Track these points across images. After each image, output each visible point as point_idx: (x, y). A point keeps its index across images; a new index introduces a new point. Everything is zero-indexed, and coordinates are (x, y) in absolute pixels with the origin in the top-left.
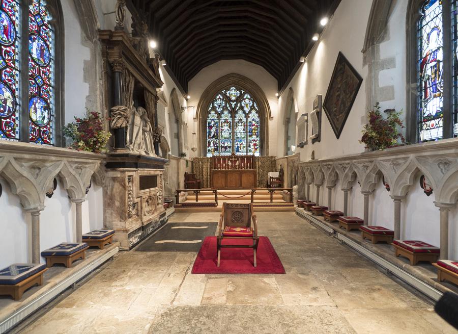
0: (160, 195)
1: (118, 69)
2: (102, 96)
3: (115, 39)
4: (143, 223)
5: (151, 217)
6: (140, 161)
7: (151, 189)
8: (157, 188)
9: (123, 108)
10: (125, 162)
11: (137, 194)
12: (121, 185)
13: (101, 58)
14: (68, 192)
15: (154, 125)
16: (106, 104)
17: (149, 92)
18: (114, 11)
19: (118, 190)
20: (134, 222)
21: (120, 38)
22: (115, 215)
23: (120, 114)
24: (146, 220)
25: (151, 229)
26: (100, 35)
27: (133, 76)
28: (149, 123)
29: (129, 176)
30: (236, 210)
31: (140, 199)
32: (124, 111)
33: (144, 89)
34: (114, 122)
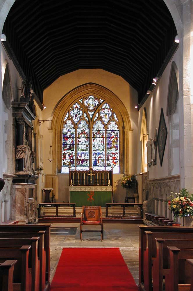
3: (21, 106)
9: (24, 147)
12: (22, 193)
19: (20, 197)
22: (17, 212)
34: (19, 155)
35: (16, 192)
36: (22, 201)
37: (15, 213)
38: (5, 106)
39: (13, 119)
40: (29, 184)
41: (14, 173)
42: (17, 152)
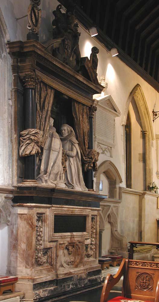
0: (91, 244)
1: (30, 84)
2: (11, 118)
3: (26, 50)
4: (57, 275)
5: (72, 271)
6: (55, 195)
7: (75, 233)
8: (85, 233)
9: (33, 132)
10: (33, 196)
11: (49, 236)
12: (28, 223)
13: (11, 73)
14: (111, 225)
15: (87, 147)
16: (15, 128)
17: (79, 103)
18: (26, 15)
19: (25, 230)
20: (44, 272)
21: (31, 49)
22: (21, 260)
23: (29, 139)
24: (62, 273)
25: (71, 286)
26: (10, 48)
27: (52, 88)
28: (77, 146)
29: (92, 215)
30: (144, 271)
31: (54, 244)
32: (34, 135)
33: (71, 101)
34: (23, 148)
35: (19, 220)
42: (21, 143)
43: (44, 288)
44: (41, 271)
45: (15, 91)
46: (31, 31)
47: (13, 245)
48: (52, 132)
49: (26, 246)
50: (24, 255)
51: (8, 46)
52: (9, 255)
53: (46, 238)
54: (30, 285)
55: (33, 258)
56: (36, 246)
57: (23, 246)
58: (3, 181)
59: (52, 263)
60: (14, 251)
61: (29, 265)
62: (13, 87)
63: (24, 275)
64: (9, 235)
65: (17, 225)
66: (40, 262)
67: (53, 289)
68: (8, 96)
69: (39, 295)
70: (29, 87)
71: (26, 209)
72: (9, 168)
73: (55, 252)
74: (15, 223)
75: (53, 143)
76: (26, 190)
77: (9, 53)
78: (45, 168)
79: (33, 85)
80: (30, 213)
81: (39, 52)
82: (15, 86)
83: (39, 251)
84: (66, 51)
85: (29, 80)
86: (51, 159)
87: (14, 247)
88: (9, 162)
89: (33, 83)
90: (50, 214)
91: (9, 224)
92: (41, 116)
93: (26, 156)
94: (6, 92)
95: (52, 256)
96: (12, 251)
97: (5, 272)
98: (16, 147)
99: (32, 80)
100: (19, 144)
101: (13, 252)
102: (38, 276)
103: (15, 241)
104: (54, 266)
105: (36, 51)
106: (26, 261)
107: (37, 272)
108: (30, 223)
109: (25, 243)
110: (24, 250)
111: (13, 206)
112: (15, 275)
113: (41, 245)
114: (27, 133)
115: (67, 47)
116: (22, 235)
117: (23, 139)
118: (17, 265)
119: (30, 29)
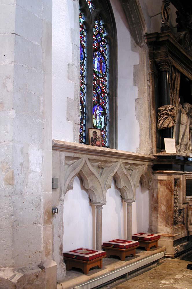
1: (165, 67)
3: (161, 40)
9: (170, 108)
11: (183, 199)
12: (168, 188)
13: (149, 59)
19: (164, 194)
21: (166, 38)
22: (161, 220)
26: (147, 38)
27: (179, 72)
34: (161, 122)
35: (159, 185)
36: (167, 202)
37: (157, 221)
38: (134, 41)
39: (150, 63)
40: (186, 172)
41: (155, 153)
42: (159, 118)
43: (180, 244)
44: (177, 229)
45: (152, 74)
46: (164, 25)
47: (154, 207)
48: (180, 109)
49: (166, 208)
50: (164, 216)
51: (146, 37)
52: (151, 216)
53: (181, 201)
54: (171, 241)
55: (172, 218)
56: (174, 208)
57: (163, 208)
58: (145, 151)
59: (184, 222)
60: (155, 212)
61: (169, 225)
62: (150, 71)
63: (164, 233)
64: (150, 198)
65: (157, 189)
66: (177, 222)
67: (186, 244)
68: (147, 78)
69: (177, 250)
70: (164, 70)
71: (165, 176)
72: (150, 140)
73: (186, 213)
74: (155, 188)
75: (181, 118)
76: (165, 159)
77: (146, 43)
78: (177, 139)
79: (168, 68)
80: (169, 179)
81: (172, 42)
82: (151, 69)
83: (176, 212)
84: (186, 42)
85: (164, 64)
86: (181, 132)
87: (155, 209)
88: (149, 135)
89: (167, 67)
90: (183, 180)
91: (150, 189)
92: (173, 94)
93: (164, 129)
94: (146, 75)
95: (184, 216)
96: (153, 212)
97: (147, 230)
98: (154, 122)
99: (167, 64)
100: (157, 119)
101: (154, 213)
102: (176, 234)
103: (156, 204)
104: (186, 224)
105: (170, 40)
106: (166, 221)
107: (175, 231)
108: (170, 188)
109: (164, 206)
110: (164, 211)
111: (153, 173)
112: (156, 233)
113: (177, 206)
114: (164, 108)
115: (187, 39)
116: (161, 198)
117: (161, 114)
118: (157, 225)
119: (163, 23)
